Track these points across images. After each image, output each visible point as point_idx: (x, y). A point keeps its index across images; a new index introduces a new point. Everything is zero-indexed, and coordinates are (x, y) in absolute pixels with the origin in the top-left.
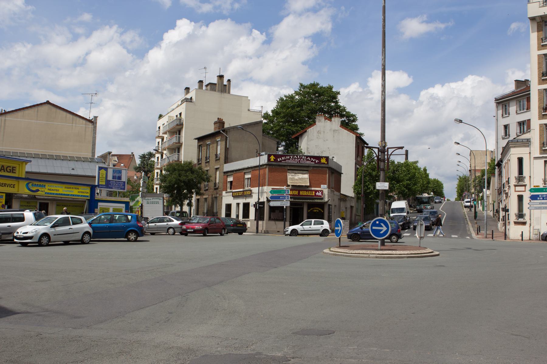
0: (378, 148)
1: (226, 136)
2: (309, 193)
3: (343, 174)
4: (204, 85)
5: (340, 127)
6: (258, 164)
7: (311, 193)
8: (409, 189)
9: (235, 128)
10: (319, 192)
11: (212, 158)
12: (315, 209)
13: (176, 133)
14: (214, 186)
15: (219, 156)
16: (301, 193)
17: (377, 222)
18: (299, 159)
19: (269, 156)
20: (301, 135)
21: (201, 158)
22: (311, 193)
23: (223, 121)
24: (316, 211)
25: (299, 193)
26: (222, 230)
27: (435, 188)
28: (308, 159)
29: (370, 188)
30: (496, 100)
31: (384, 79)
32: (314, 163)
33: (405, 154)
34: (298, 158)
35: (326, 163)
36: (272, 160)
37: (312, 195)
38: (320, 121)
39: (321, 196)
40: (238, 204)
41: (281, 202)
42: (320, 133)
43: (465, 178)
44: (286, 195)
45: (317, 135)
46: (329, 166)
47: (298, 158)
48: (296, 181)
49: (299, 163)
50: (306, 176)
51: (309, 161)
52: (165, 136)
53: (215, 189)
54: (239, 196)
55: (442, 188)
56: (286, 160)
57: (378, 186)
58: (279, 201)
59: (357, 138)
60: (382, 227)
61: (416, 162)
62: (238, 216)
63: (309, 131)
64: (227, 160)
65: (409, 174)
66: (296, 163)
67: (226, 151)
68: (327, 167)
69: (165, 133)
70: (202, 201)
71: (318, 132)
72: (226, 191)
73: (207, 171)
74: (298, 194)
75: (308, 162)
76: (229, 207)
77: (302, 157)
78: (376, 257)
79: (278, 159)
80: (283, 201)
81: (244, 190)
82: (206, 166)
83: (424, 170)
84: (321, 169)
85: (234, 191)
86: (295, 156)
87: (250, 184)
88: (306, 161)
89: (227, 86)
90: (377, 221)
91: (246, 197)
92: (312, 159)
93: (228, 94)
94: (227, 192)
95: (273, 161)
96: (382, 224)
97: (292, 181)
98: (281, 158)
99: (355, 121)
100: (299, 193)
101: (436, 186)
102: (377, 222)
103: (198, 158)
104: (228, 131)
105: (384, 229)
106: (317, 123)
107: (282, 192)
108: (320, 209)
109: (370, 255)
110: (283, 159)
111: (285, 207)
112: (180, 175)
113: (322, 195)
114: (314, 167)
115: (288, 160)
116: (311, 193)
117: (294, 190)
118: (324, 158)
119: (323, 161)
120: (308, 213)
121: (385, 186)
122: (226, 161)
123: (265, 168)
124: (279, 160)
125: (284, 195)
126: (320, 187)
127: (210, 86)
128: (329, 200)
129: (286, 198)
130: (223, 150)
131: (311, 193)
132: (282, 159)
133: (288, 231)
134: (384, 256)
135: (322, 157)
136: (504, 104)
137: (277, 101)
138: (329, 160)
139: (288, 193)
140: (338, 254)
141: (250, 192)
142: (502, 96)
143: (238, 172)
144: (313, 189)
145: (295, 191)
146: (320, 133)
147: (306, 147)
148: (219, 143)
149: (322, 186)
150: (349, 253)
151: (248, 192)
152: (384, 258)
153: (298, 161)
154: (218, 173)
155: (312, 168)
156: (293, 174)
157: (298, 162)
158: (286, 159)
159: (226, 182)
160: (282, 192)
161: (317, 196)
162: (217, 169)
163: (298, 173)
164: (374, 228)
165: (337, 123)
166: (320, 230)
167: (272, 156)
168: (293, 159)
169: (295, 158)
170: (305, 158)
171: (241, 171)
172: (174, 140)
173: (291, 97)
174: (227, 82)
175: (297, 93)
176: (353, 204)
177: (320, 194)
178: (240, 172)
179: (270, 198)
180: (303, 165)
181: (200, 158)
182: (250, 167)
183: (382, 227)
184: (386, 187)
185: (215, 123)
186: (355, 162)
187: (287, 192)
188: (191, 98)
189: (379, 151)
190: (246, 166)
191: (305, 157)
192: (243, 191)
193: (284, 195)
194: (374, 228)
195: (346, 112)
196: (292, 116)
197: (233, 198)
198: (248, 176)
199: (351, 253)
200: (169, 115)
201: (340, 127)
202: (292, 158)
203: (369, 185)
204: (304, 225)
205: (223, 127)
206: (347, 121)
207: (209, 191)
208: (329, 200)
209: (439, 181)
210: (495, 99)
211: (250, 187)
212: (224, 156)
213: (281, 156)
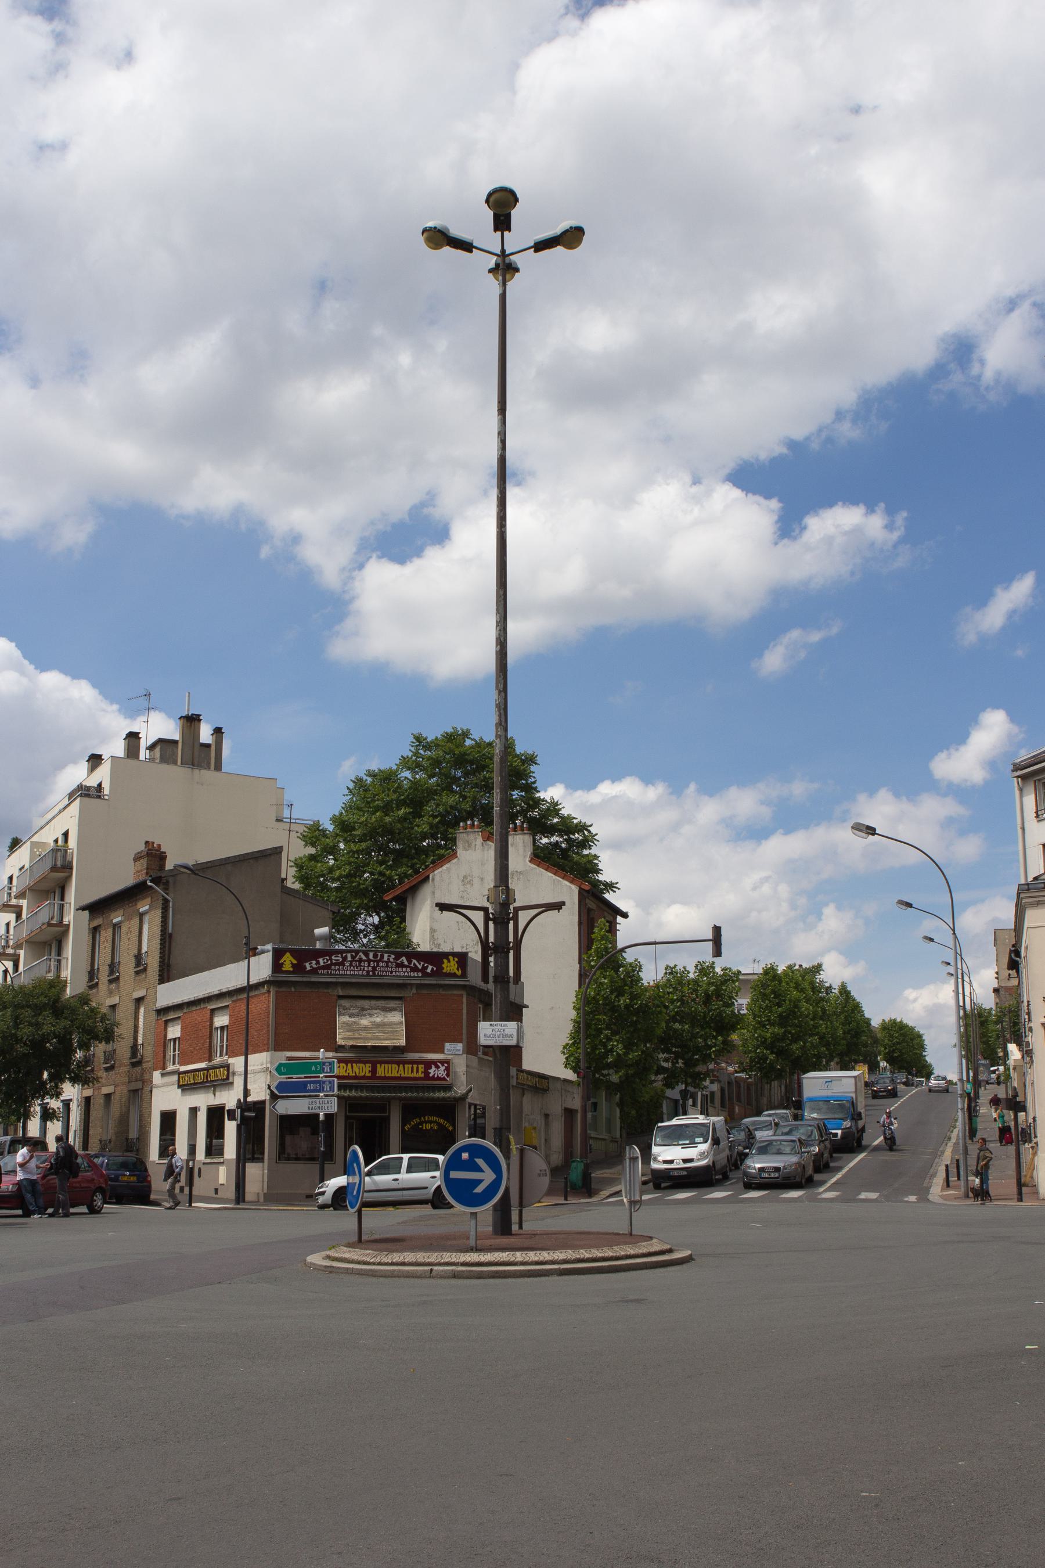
0: (485, 910)
1: (163, 896)
2: (407, 1072)
3: (527, 1007)
4: (143, 744)
5: (530, 862)
6: (242, 982)
7: (412, 1068)
8: (780, 1053)
9: (201, 871)
10: (437, 1067)
11: (127, 967)
12: (426, 1122)
13: (55, 893)
14: (129, 1055)
15: (145, 959)
16: (381, 1070)
17: (463, 1154)
18: (374, 961)
19: (278, 954)
20: (414, 890)
21: (98, 969)
22: (412, 1068)
23: (162, 850)
24: (428, 1126)
25: (374, 1071)
26: (94, 1194)
27: (896, 1049)
28: (402, 963)
29: (612, 1049)
30: (1017, 768)
31: (501, 687)
32: (420, 974)
33: (710, 937)
34: (369, 961)
35: (459, 973)
36: (288, 967)
37: (415, 1075)
38: (469, 846)
39: (444, 1079)
40: (194, 1111)
41: (311, 1100)
42: (469, 882)
43: (980, 1015)
44: (326, 1077)
45: (462, 889)
46: (467, 983)
47: (369, 961)
48: (363, 1034)
49: (374, 974)
50: (397, 1018)
51: (404, 969)
52: (24, 903)
53: (134, 1065)
54: (195, 1084)
55: (922, 1047)
56: (333, 967)
57: (485, 1035)
58: (305, 1096)
59: (585, 894)
60: (480, 1170)
61: (817, 968)
62: (192, 1150)
63: (437, 878)
64: (168, 971)
65: (779, 1005)
66: (363, 975)
67: (165, 942)
68: (464, 987)
69: (21, 895)
70: (98, 1104)
71: (463, 881)
72: (164, 1068)
73: (113, 1007)
74: (370, 1075)
75: (402, 972)
76: (168, 1119)
77: (382, 956)
78: (455, 1275)
79: (307, 965)
80: (316, 1096)
81: (210, 1064)
82: (111, 993)
83: (840, 992)
84: (444, 993)
85: (183, 1068)
86: (361, 954)
87: (227, 1045)
88: (394, 969)
89: (213, 748)
90: (465, 1151)
91: (215, 1086)
92: (414, 961)
93: (217, 773)
94: (164, 1072)
95: (291, 969)
96: (480, 1162)
97: (350, 1034)
98: (314, 962)
99: (590, 845)
100: (374, 1071)
101: (898, 1043)
102: (465, 1156)
103: (89, 969)
104: (171, 880)
105: (488, 1176)
106: (460, 852)
107: (313, 1068)
108: (442, 1121)
109: (435, 1268)
110: (322, 964)
111: (322, 1117)
112: (17, 1021)
113: (448, 1075)
114: (420, 986)
115: (337, 967)
116: (412, 1071)
117: (357, 1062)
118: (451, 958)
119: (450, 966)
120: (404, 1134)
121: (506, 1035)
122: (165, 975)
123: (264, 993)
124: (308, 968)
125: (319, 1077)
126: (442, 1052)
127: (162, 750)
128: (470, 1090)
129: (327, 1087)
130: (157, 942)
131: (412, 1071)
132: (318, 963)
133: (323, 1193)
134: (482, 1271)
135: (446, 955)
136: (1039, 780)
137: (348, 788)
138: (469, 963)
139: (332, 1070)
140: (339, 1268)
141: (226, 1073)
142: (1034, 756)
143: (194, 1008)
144: (416, 1056)
145: (361, 1065)
146: (470, 883)
147: (428, 929)
148: (146, 918)
149: (447, 1046)
150: (373, 1264)
151: (220, 1071)
152: (480, 1276)
153: (370, 969)
154: (142, 1010)
155: (414, 991)
156: (356, 1011)
157: (371, 973)
158: (332, 964)
159: (165, 1041)
160: (313, 1068)
161: (433, 1078)
162: (139, 1001)
163: (372, 1008)
164: (454, 1175)
165: (521, 851)
166: (426, 1188)
167: (288, 955)
168: (354, 963)
169: (360, 960)
170: (392, 960)
171: (202, 1006)
172: (46, 912)
173: (386, 778)
174: (212, 735)
175: (405, 763)
176: (576, 1103)
177: (441, 1072)
178: (198, 1008)
179: (277, 1088)
180: (386, 981)
181: (96, 967)
182: (224, 990)
183: (480, 1170)
184: (511, 1036)
185: (137, 858)
186: (580, 971)
187: (327, 1068)
188: (100, 785)
189: (487, 919)
190: (214, 990)
191: (393, 956)
192: (207, 1069)
193: (319, 1077)
194: (454, 1175)
195: (562, 818)
196: (389, 831)
197: (180, 1090)
198: (221, 1020)
199: (380, 1264)
200: (31, 840)
201: (530, 864)
202: (349, 958)
203: (609, 1039)
204: (374, 1175)
205: (162, 866)
206: (563, 845)
207: (116, 1070)
208: (470, 1090)
209: (906, 1026)
210: (1014, 765)
211: (226, 1054)
212: (157, 958)
213: (318, 954)
